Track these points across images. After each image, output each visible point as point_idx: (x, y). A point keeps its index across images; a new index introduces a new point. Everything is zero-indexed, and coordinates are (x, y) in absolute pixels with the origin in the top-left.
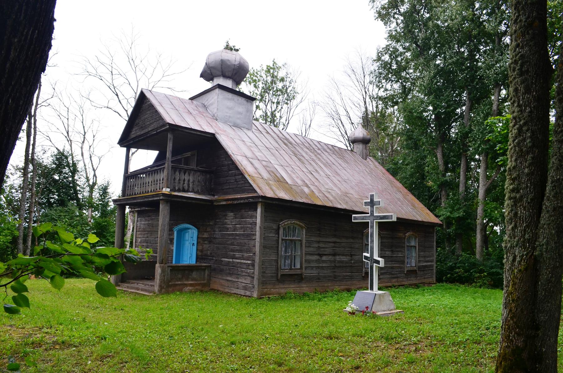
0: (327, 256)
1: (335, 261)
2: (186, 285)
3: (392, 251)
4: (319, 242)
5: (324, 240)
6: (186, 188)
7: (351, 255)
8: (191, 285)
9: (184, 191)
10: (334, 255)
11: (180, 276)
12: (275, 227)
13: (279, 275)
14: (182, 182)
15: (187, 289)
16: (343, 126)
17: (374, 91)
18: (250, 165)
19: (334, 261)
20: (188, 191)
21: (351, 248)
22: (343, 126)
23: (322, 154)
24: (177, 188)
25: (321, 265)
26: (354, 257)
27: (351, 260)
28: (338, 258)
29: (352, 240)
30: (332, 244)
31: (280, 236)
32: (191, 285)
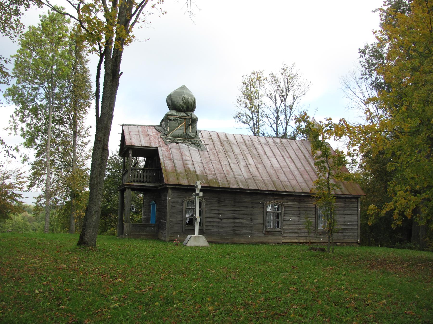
0: (227, 220)
1: (234, 223)
2: (142, 235)
3: (299, 217)
4: (219, 210)
5: (224, 209)
6: (142, 180)
7: (251, 219)
8: (145, 235)
9: (140, 182)
10: (234, 218)
11: (138, 230)
12: (180, 201)
13: (184, 229)
14: (139, 177)
15: (142, 237)
16: (302, 152)
17: (4, 104)
18: (300, 176)
19: (234, 223)
20: (143, 182)
21: (251, 214)
22: (302, 152)
23: (301, 169)
24: (136, 181)
25: (220, 225)
26: (254, 221)
27: (252, 222)
28: (237, 221)
29: (252, 209)
30: (232, 212)
31: (184, 207)
32: (145, 235)
